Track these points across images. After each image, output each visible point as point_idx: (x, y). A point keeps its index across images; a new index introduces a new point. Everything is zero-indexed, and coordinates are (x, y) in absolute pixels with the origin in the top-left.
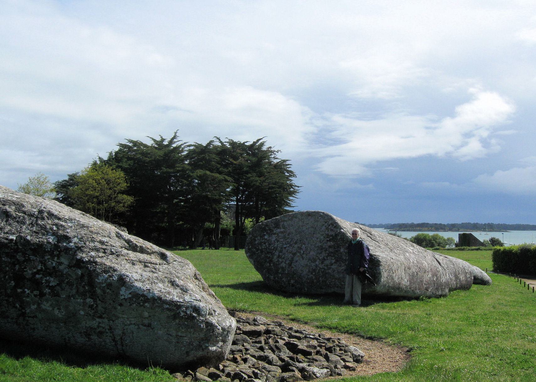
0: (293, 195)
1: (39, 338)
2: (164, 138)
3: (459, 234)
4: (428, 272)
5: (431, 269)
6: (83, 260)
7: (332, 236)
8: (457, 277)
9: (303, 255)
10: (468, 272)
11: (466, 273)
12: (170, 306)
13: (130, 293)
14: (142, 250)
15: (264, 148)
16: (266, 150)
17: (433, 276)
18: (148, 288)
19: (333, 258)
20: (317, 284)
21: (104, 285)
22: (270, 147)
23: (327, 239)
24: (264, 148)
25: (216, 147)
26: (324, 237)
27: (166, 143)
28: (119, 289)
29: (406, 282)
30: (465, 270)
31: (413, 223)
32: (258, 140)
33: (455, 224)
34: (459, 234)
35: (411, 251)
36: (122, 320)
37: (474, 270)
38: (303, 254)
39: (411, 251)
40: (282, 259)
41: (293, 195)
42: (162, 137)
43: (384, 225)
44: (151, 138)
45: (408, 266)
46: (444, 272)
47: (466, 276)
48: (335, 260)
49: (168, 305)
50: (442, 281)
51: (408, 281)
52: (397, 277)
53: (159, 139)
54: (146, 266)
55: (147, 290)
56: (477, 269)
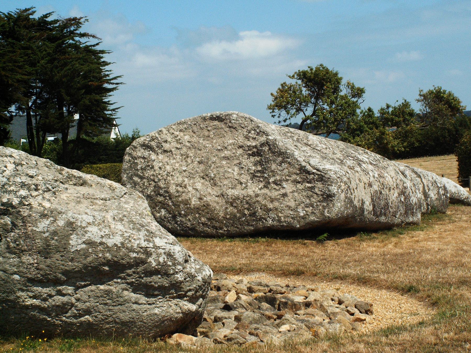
1: (157, 267)
4: (393, 189)
6: (12, 204)
7: (255, 147)
10: (441, 187)
11: (439, 188)
12: (138, 254)
13: (84, 242)
14: (84, 183)
18: (107, 233)
19: (261, 179)
20: (15, 273)
21: (47, 234)
28: (68, 237)
29: (368, 206)
30: (437, 184)
35: (367, 160)
36: (73, 281)
39: (367, 160)
40: (183, 189)
45: (368, 181)
46: (413, 188)
49: (136, 252)
50: (412, 201)
51: (370, 204)
52: (356, 199)
54: (93, 204)
55: (105, 235)
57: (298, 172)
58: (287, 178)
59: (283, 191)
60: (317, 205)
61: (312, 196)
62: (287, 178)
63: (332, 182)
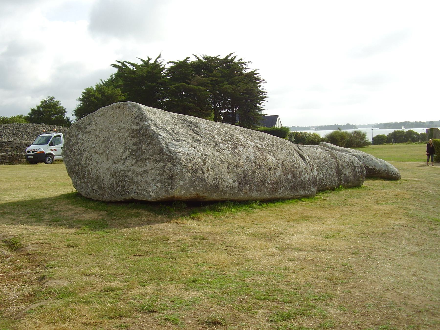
0: (264, 100)
2: (150, 58)
3: (427, 129)
5: (283, 165)
8: (339, 171)
9: (108, 155)
11: (355, 167)
15: (236, 61)
16: (237, 62)
17: (286, 173)
19: (134, 157)
22: (241, 59)
23: (132, 135)
24: (236, 61)
25: (193, 64)
26: (130, 133)
27: (152, 62)
30: (353, 164)
31: (397, 122)
32: (230, 54)
33: (433, 121)
34: (427, 129)
37: (378, 163)
38: (108, 154)
41: (264, 100)
42: (148, 57)
43: (372, 125)
44: (141, 59)
47: (354, 170)
48: (135, 160)
53: (146, 59)
56: (381, 162)
57: (158, 153)
58: (150, 157)
59: (145, 168)
60: (164, 182)
61: (162, 174)
62: (150, 157)
63: (177, 163)
